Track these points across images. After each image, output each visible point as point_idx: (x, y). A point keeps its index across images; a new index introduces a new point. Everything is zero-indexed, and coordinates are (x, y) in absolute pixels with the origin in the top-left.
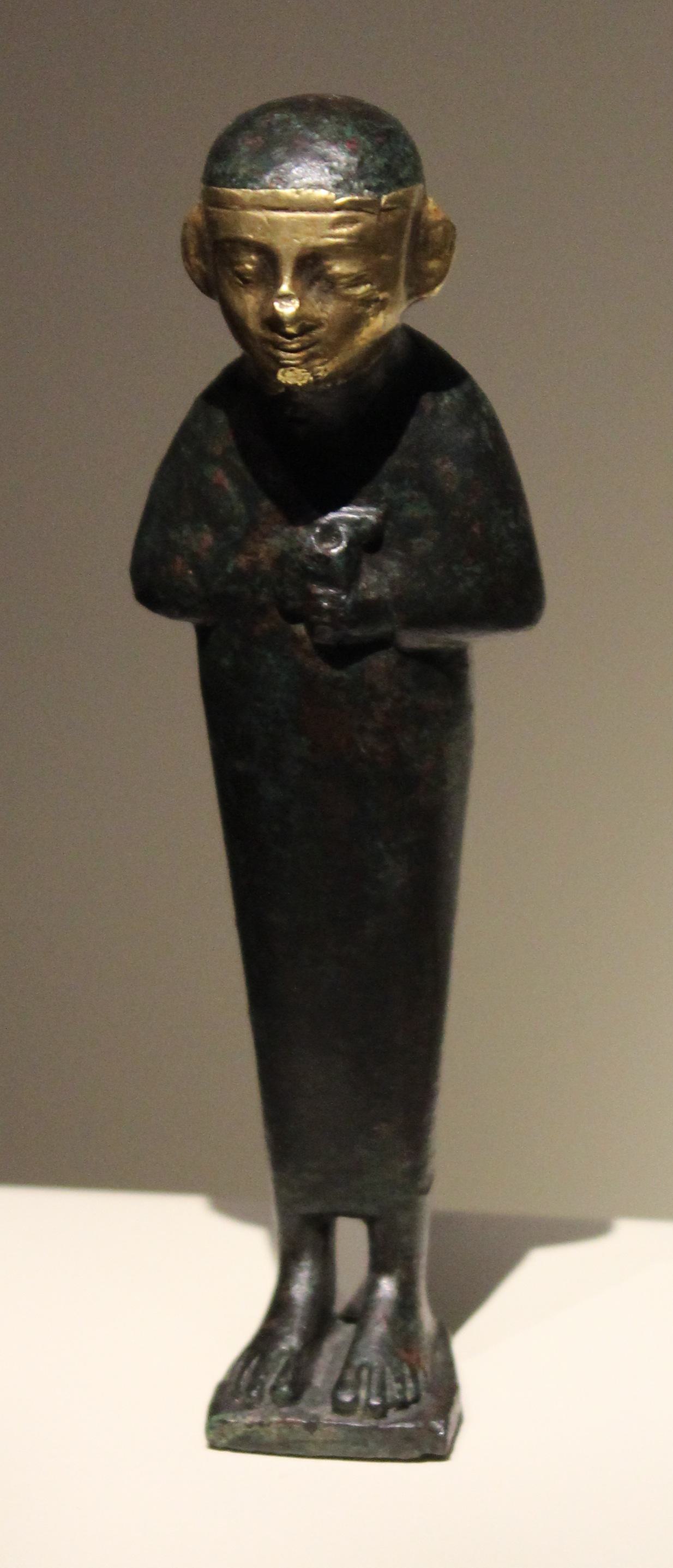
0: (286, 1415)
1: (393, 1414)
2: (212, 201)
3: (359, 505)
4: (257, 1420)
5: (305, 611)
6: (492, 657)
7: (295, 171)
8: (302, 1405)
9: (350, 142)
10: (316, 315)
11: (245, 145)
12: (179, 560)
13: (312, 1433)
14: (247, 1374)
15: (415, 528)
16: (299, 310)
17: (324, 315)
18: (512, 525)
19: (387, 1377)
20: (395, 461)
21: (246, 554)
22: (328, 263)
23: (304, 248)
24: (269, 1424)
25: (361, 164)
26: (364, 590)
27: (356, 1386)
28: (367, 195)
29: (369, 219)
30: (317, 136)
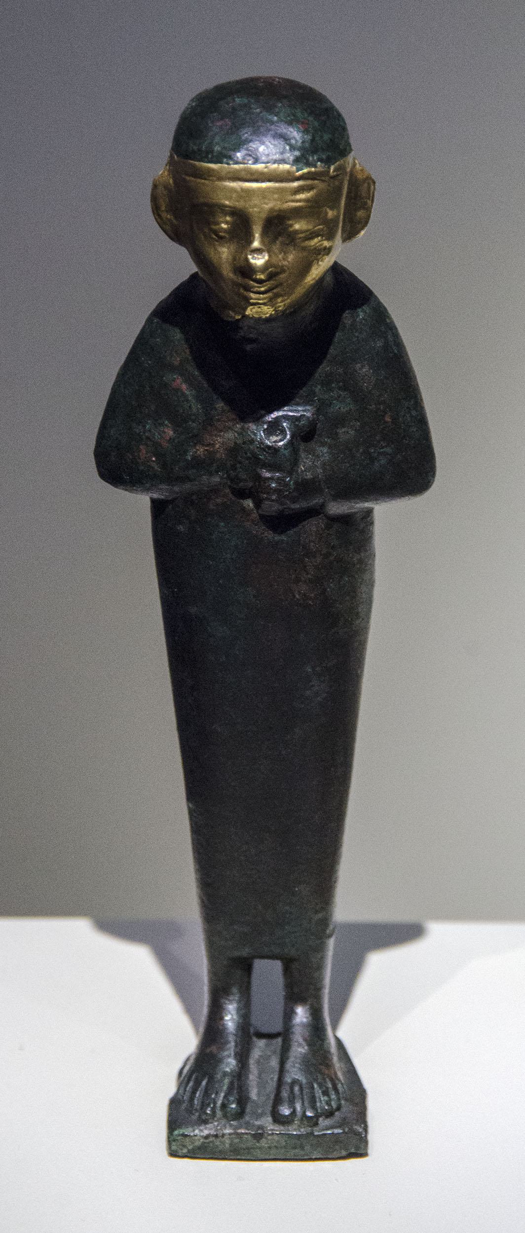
0: (236, 1128)
3: (298, 404)
4: (213, 1132)
8: (247, 1118)
9: (303, 123)
11: (216, 127)
13: (258, 1142)
15: (340, 421)
16: (267, 262)
17: (285, 263)
18: (414, 413)
19: (316, 1091)
20: (325, 368)
21: (203, 445)
23: (271, 210)
24: (223, 1135)
27: (291, 1103)
30: (276, 118)
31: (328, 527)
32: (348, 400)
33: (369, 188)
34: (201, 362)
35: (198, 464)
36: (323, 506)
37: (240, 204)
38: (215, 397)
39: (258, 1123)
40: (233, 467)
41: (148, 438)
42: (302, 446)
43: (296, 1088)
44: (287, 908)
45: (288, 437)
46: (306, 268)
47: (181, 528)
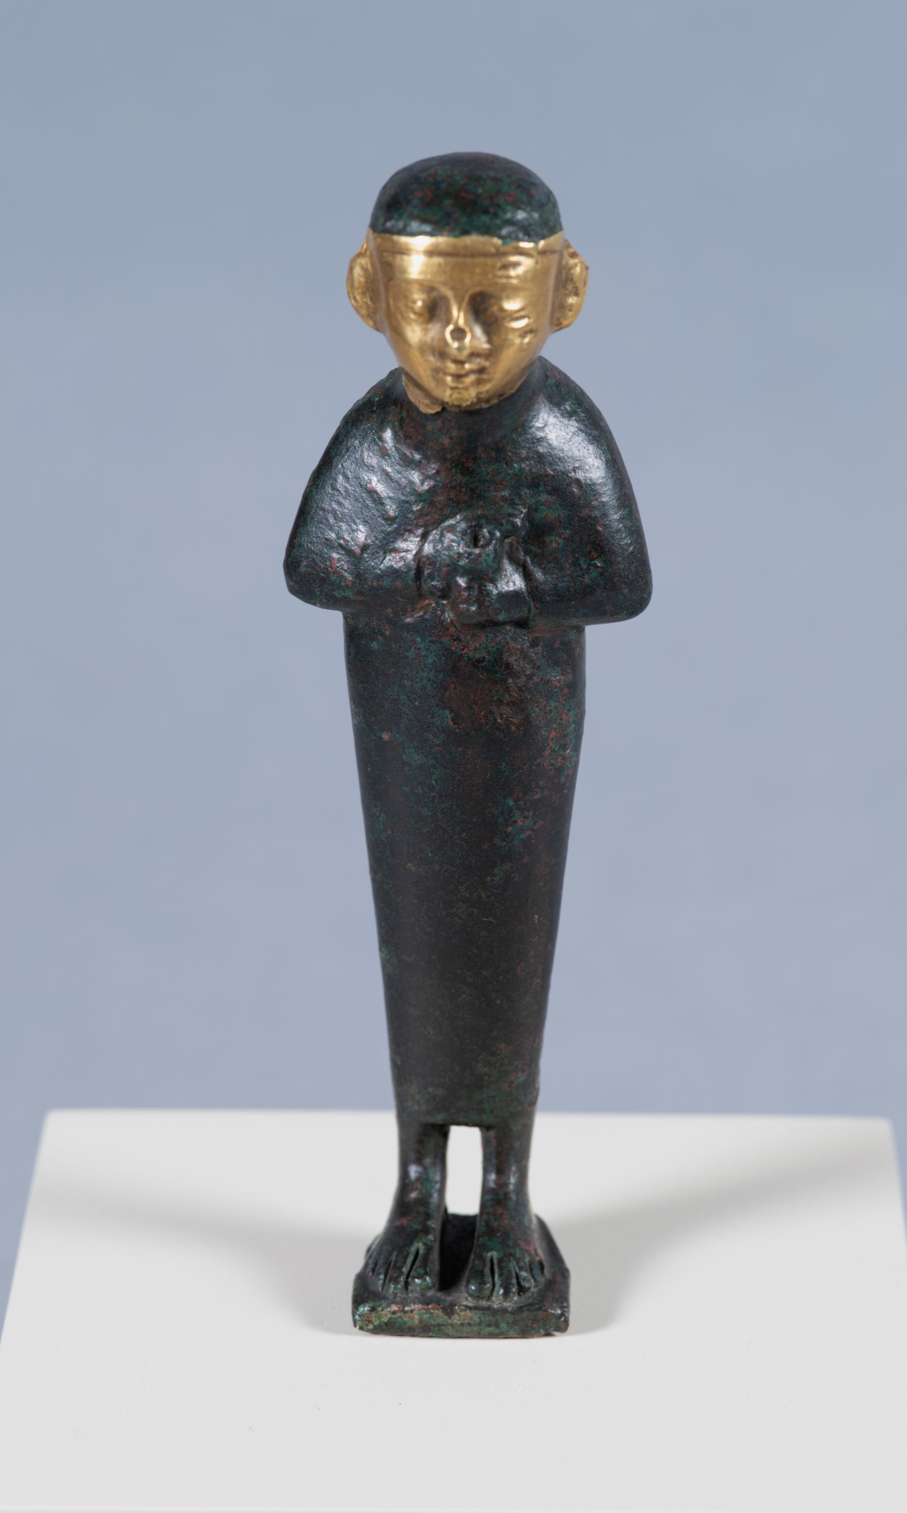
13: (450, 1318)
44: (486, 1069)
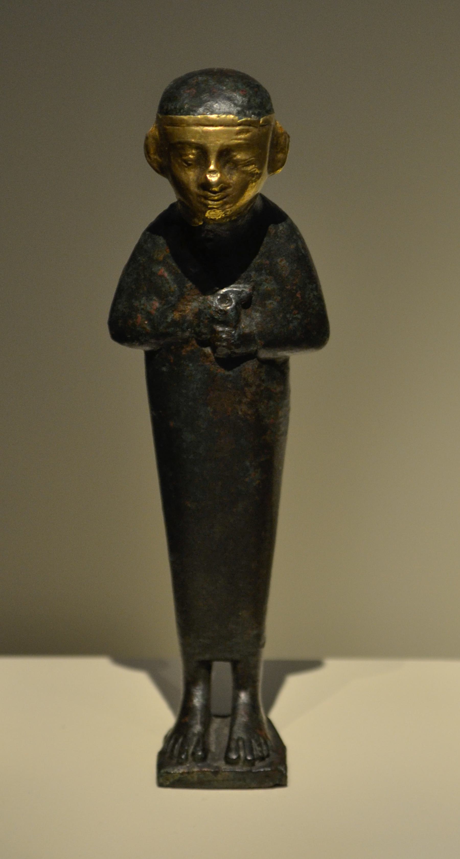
1: (258, 764)
2: (160, 124)
3: (240, 283)
4: (186, 771)
5: (212, 340)
6: (300, 363)
7: (216, 106)
8: (208, 761)
9: (242, 91)
10: (228, 182)
11: (185, 99)
12: (139, 315)
14: (177, 746)
15: (267, 295)
16: (220, 178)
17: (232, 181)
18: (315, 293)
20: (257, 260)
21: (178, 311)
22: (235, 154)
23: (222, 145)
24: (193, 772)
25: (249, 101)
26: (243, 328)
27: (237, 751)
28: (253, 118)
29: (254, 130)
30: (225, 88)
31: (260, 367)
32: (273, 282)
33: (285, 139)
34: (176, 256)
35: (175, 323)
36: (256, 352)
37: (202, 141)
38: (186, 279)
39: (215, 764)
40: (198, 326)
41: (142, 309)
42: (243, 311)
43: (241, 743)
45: (234, 303)
46: (243, 188)
47: (164, 369)
